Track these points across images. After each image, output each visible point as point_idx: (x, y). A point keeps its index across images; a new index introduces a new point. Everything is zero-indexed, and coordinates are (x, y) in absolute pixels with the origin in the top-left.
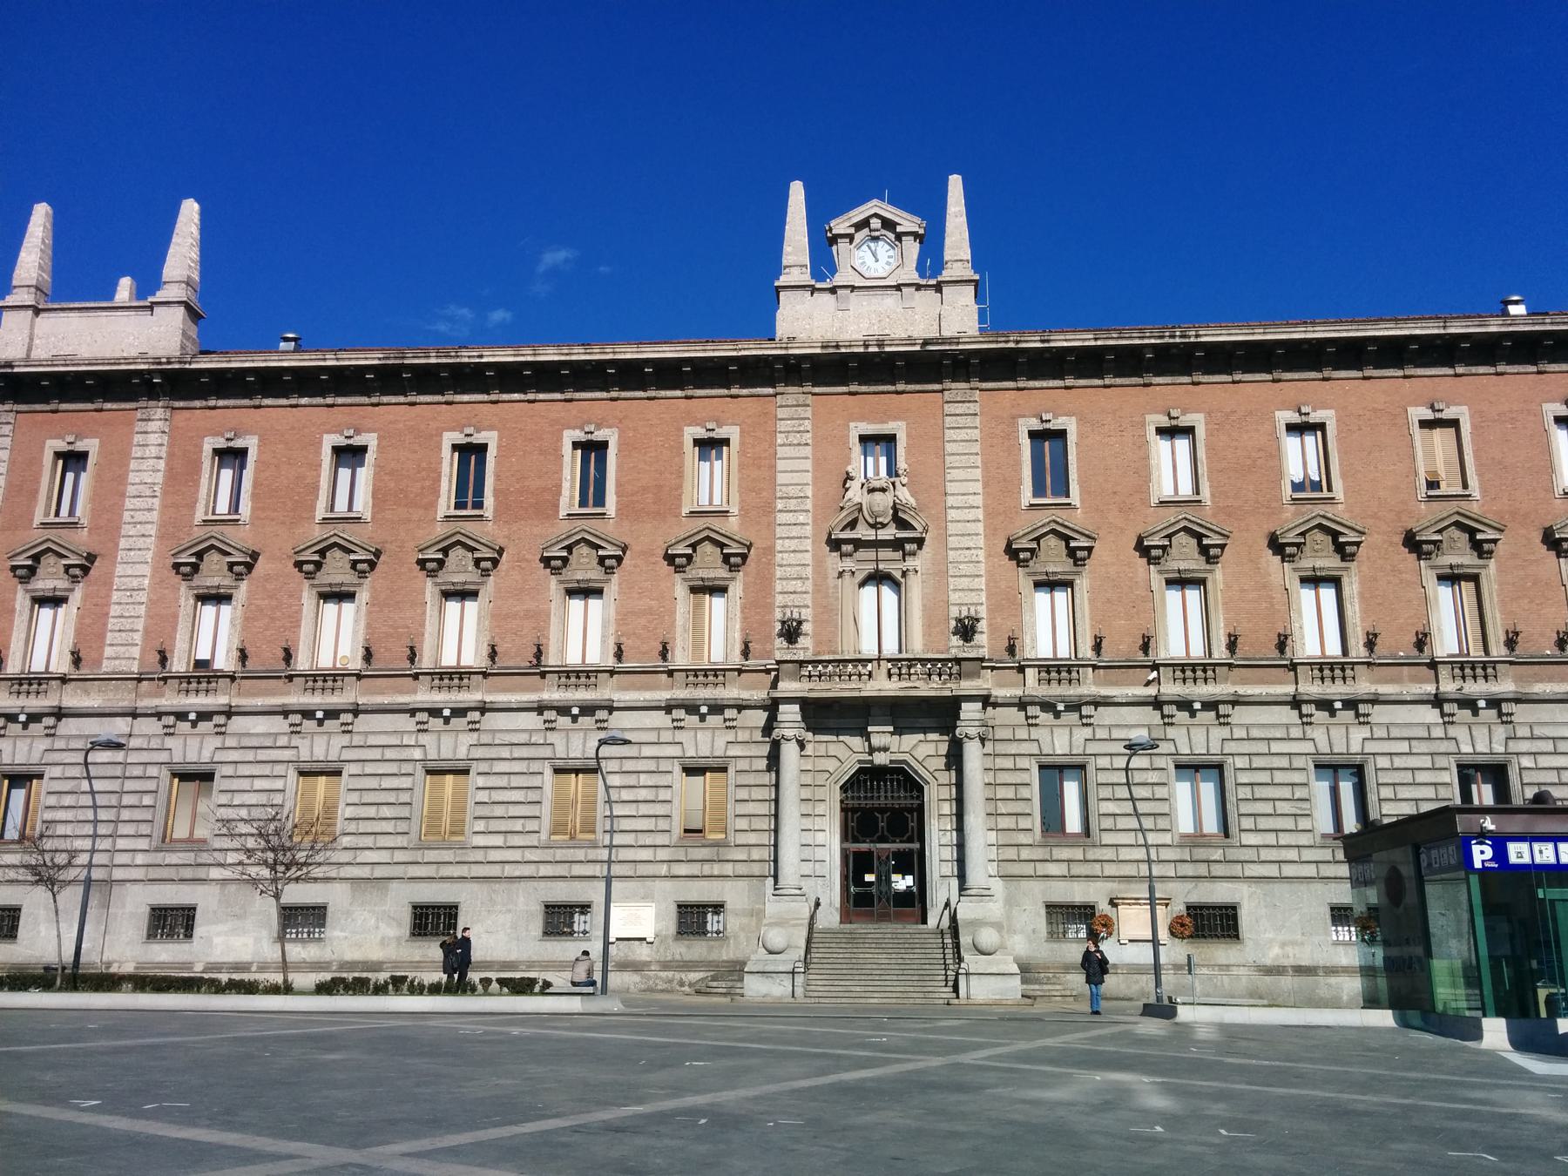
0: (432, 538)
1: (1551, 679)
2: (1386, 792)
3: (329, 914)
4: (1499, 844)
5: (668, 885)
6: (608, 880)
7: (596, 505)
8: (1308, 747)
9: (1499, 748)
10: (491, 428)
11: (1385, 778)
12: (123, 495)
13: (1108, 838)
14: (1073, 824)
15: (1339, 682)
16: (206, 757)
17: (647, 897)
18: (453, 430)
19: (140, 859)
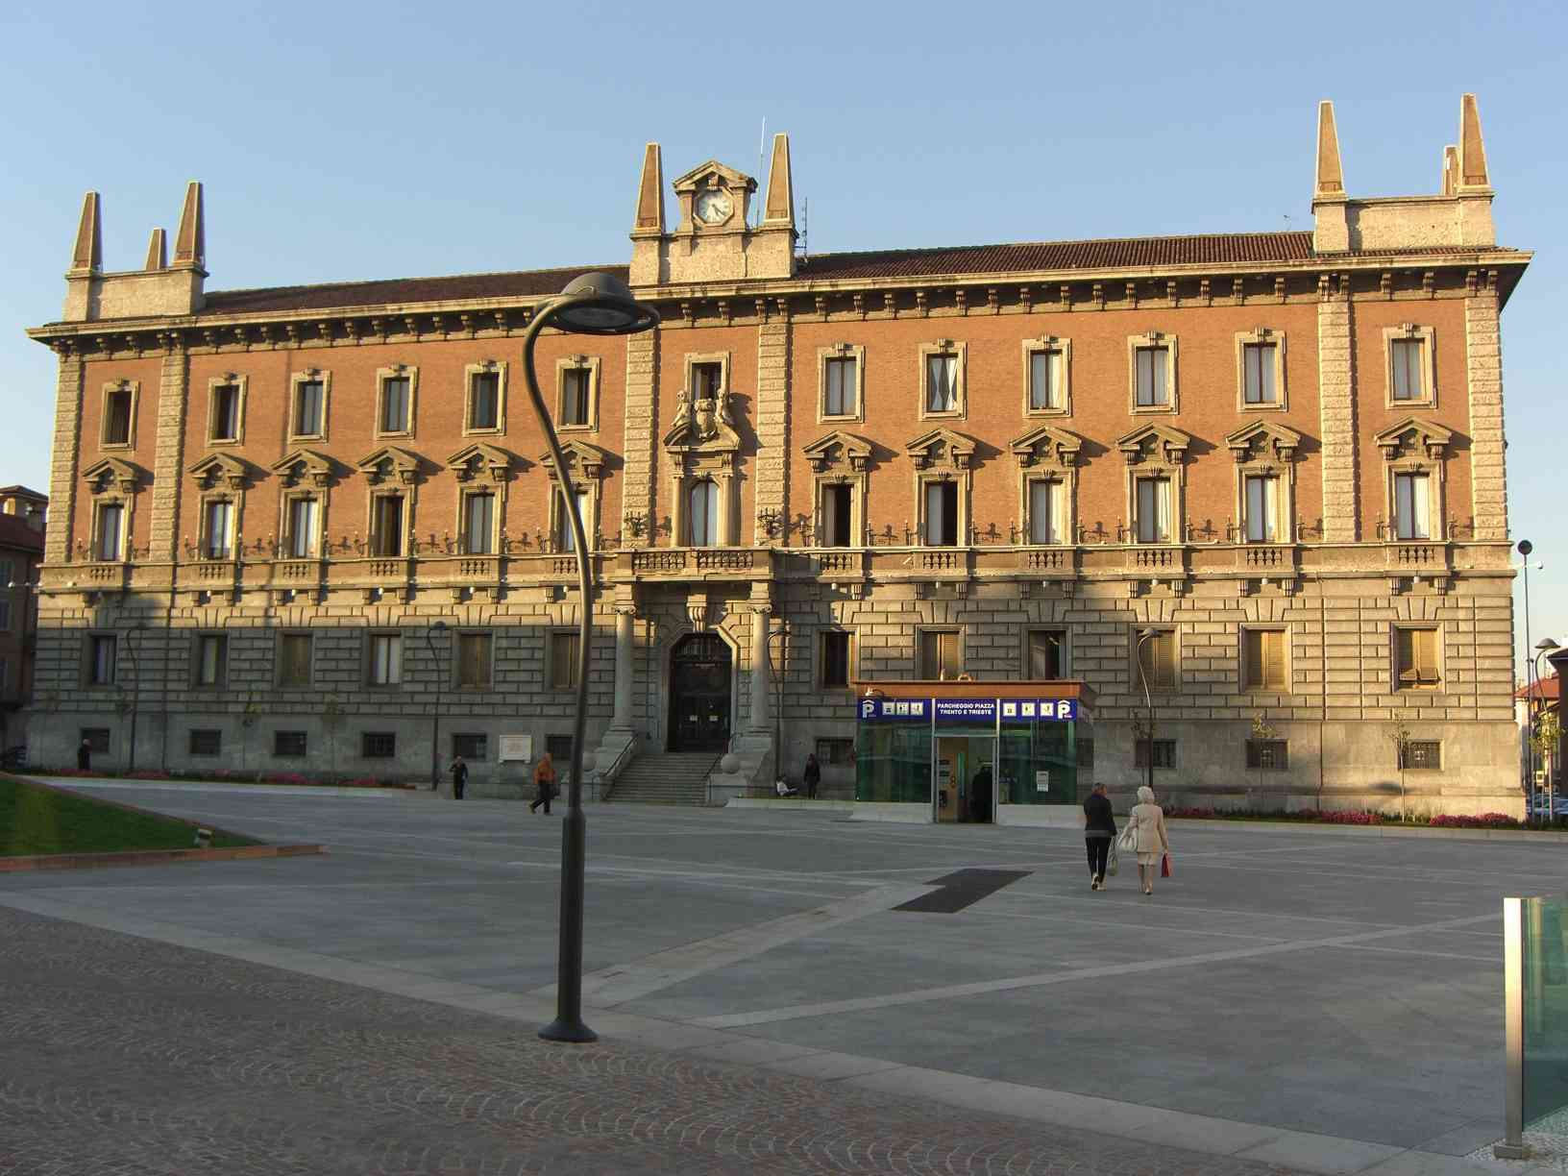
0: (370, 454)
1: (1213, 563)
2: (76, 655)
3: (397, 744)
4: (879, 701)
5: (542, 722)
6: (436, 717)
7: (579, 422)
8: (1023, 618)
9: (1166, 617)
10: (554, 362)
11: (1014, 642)
12: (155, 425)
13: (232, 687)
14: (210, 676)
15: (1421, 560)
16: (1058, 618)
17: (526, 731)
18: (384, 365)
19: (182, 697)
